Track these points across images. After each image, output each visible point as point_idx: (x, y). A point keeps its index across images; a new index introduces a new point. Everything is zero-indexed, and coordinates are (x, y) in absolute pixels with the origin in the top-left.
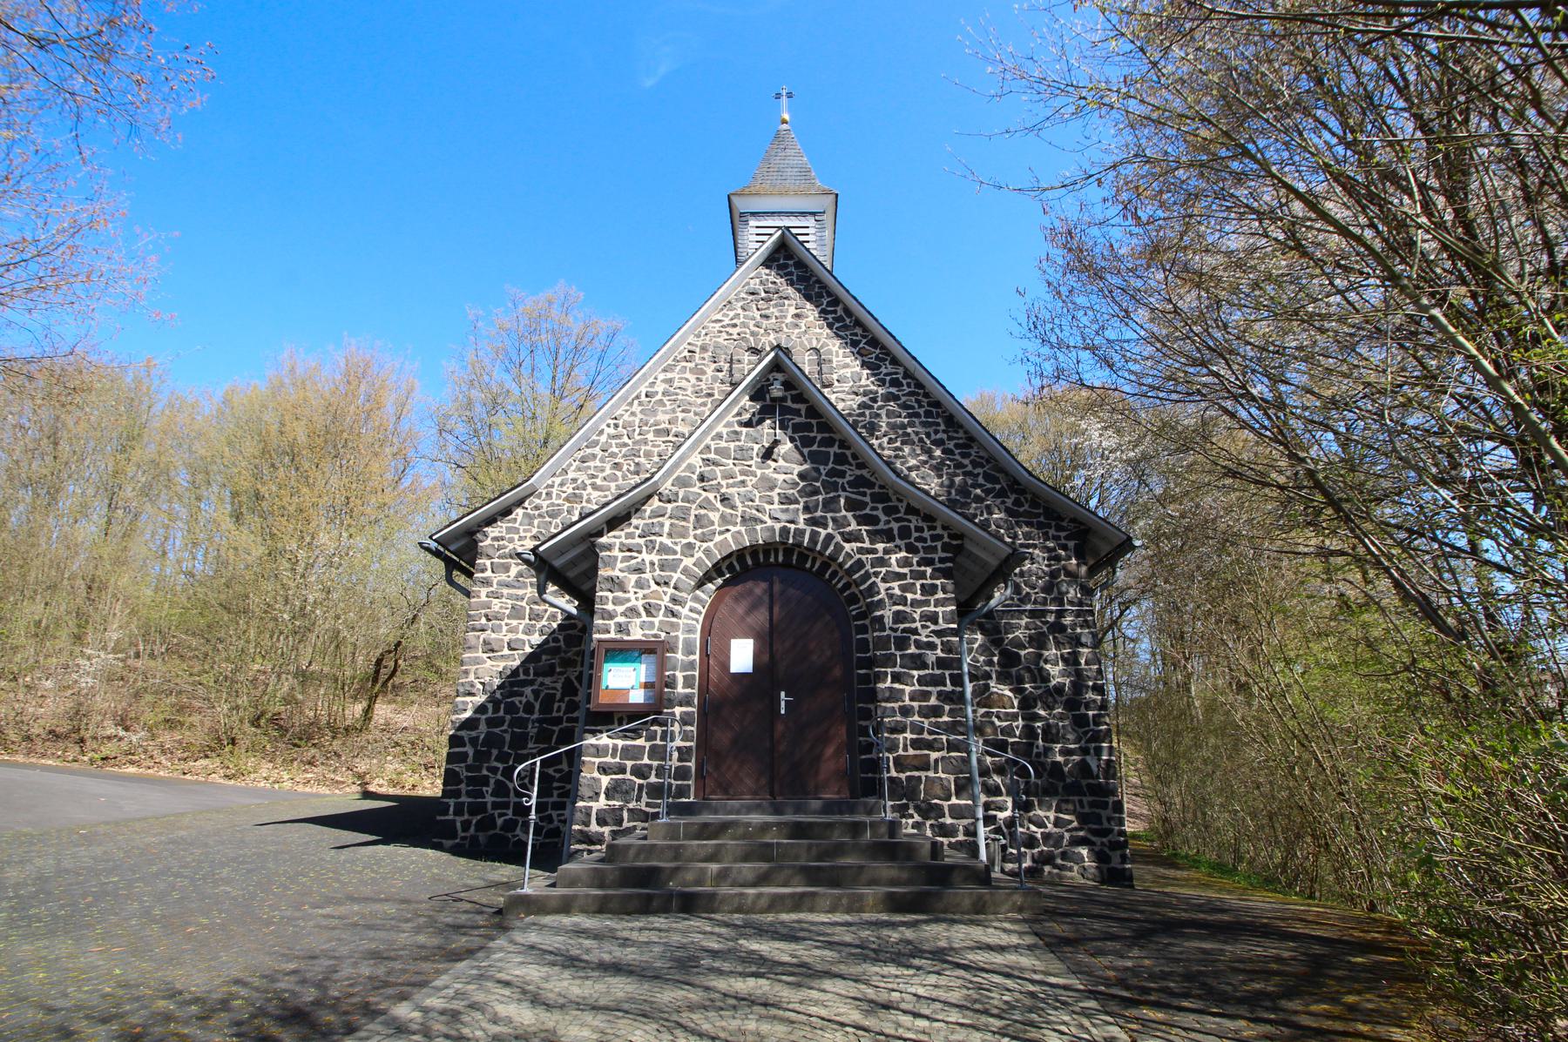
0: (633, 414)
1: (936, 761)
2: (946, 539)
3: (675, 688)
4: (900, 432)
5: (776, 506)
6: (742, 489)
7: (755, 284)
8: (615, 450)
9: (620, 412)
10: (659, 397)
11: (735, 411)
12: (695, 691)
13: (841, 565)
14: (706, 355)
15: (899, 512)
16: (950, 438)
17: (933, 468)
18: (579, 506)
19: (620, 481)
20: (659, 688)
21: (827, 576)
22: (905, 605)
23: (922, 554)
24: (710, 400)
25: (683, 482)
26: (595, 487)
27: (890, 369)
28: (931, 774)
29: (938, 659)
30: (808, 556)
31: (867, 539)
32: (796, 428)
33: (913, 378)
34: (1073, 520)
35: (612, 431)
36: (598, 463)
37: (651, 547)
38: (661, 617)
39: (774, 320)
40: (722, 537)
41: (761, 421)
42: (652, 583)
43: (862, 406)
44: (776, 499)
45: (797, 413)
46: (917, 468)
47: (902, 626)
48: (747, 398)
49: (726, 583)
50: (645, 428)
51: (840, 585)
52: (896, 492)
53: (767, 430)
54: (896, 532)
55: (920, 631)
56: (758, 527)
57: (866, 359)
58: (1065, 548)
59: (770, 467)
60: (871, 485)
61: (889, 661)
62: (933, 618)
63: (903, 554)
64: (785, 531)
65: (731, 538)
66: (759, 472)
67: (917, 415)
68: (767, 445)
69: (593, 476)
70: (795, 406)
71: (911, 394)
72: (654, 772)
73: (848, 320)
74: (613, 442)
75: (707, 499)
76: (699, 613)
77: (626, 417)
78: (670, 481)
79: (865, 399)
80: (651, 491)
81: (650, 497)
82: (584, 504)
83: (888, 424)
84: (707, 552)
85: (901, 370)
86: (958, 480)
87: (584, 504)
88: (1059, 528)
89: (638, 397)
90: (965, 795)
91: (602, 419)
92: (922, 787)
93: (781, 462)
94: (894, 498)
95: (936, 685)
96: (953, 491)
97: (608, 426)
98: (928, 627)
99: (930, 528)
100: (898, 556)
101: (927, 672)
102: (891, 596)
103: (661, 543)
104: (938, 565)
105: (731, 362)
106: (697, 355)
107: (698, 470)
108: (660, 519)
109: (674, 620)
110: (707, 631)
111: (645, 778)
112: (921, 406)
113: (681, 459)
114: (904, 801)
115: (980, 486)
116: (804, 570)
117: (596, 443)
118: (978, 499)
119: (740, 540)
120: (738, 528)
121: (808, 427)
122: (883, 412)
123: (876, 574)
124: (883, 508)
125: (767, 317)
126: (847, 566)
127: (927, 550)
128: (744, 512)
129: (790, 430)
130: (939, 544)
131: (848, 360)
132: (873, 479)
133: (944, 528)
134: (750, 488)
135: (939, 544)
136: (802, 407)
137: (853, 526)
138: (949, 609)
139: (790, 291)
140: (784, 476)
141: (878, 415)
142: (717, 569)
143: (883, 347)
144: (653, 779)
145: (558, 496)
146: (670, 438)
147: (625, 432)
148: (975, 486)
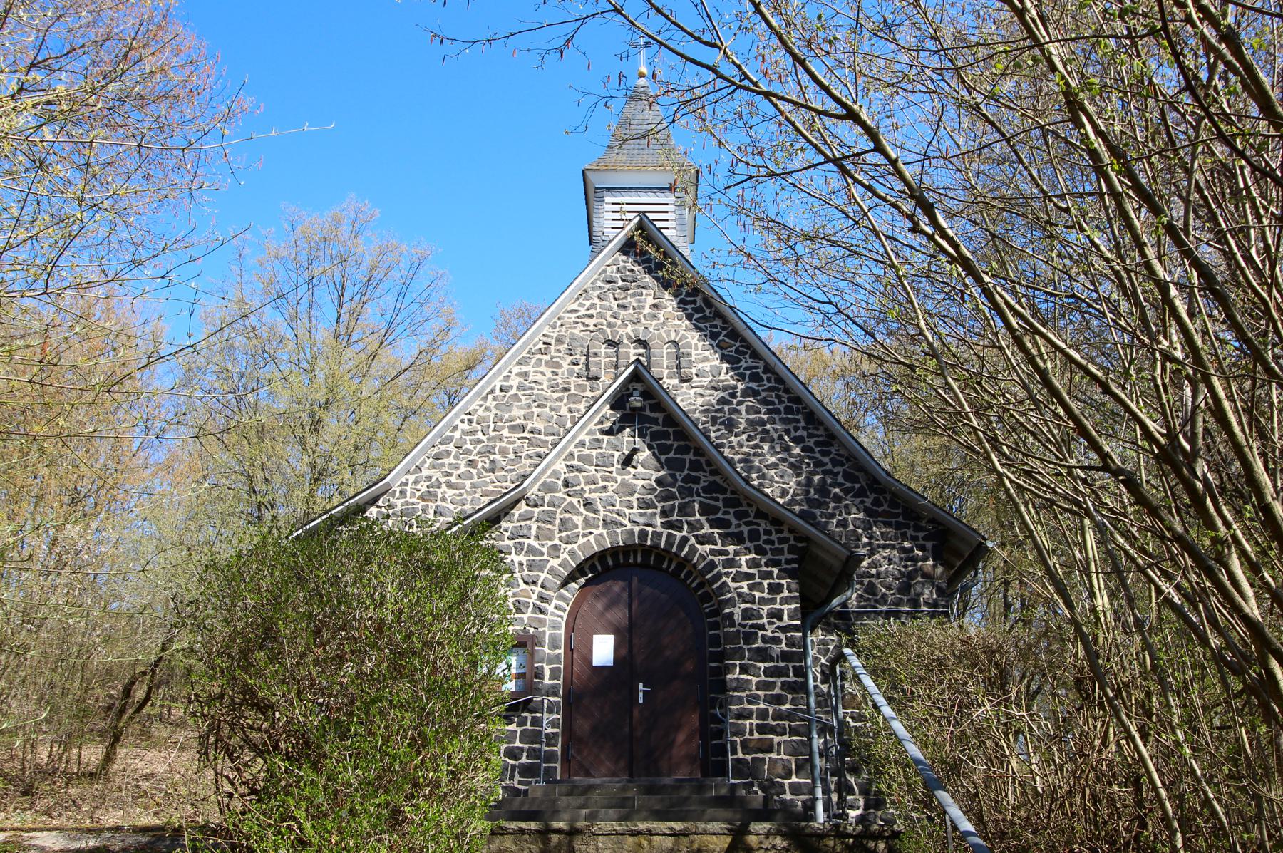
0: (487, 409)
1: (779, 744)
2: (792, 542)
3: (543, 679)
4: (760, 429)
5: (635, 510)
6: (604, 494)
7: (611, 272)
8: (470, 447)
9: (473, 407)
10: (514, 391)
11: (597, 419)
12: (561, 682)
13: (695, 566)
14: (561, 348)
15: (749, 516)
16: (810, 436)
17: (792, 466)
18: (433, 505)
19: (475, 480)
20: (530, 679)
21: (682, 576)
22: (753, 603)
23: (769, 556)
24: (566, 394)
25: (548, 488)
26: (450, 485)
27: (750, 363)
28: (774, 756)
29: (783, 652)
30: (665, 558)
31: (719, 542)
32: (655, 436)
33: (774, 373)
34: (932, 521)
35: (465, 426)
36: (452, 460)
38: (529, 614)
39: (631, 311)
40: (586, 539)
41: (621, 430)
42: (521, 582)
43: (722, 401)
44: (635, 504)
45: (655, 421)
46: (775, 466)
47: (751, 622)
48: (608, 407)
49: (588, 582)
50: (499, 424)
51: (694, 585)
52: (746, 498)
53: (627, 438)
54: (746, 535)
55: (767, 627)
56: (619, 530)
57: (726, 352)
58: (922, 548)
59: (629, 473)
60: (724, 491)
61: (739, 654)
62: (778, 615)
63: (753, 555)
64: (643, 534)
66: (619, 478)
67: (777, 411)
68: (627, 452)
69: (448, 474)
70: (653, 415)
72: (525, 754)
73: (707, 311)
74: (468, 438)
75: (571, 503)
76: (564, 610)
77: (480, 412)
78: (536, 487)
79: (723, 394)
80: (519, 496)
81: (518, 501)
82: (439, 502)
85: (761, 364)
86: (816, 478)
87: (439, 502)
89: (492, 391)
90: (803, 773)
91: (456, 416)
92: (766, 767)
93: (640, 469)
94: (744, 503)
95: (779, 676)
96: (812, 491)
97: (462, 421)
98: (773, 623)
99: (778, 532)
100: (748, 557)
101: (772, 664)
102: (740, 595)
103: (529, 545)
104: (785, 566)
105: (588, 355)
106: (552, 348)
107: (563, 477)
108: (528, 522)
109: (542, 616)
110: (571, 628)
111: (517, 759)
112: (781, 402)
113: (548, 466)
114: (750, 780)
115: (839, 485)
116: (661, 570)
117: (450, 439)
118: (837, 499)
119: (603, 543)
120: (600, 531)
121: (665, 435)
122: (743, 408)
123: (727, 574)
124: (734, 513)
125: (624, 307)
126: (700, 567)
127: (775, 552)
128: (606, 516)
129: (648, 438)
130: (785, 547)
131: (707, 353)
132: (725, 485)
133: (791, 531)
134: (611, 493)
135: (785, 547)
136: (660, 416)
137: (707, 530)
138: (793, 606)
139: (648, 279)
140: (643, 482)
141: (738, 412)
143: (743, 340)
144: (524, 760)
145: (413, 494)
146: (526, 434)
147: (479, 428)
148: (834, 485)
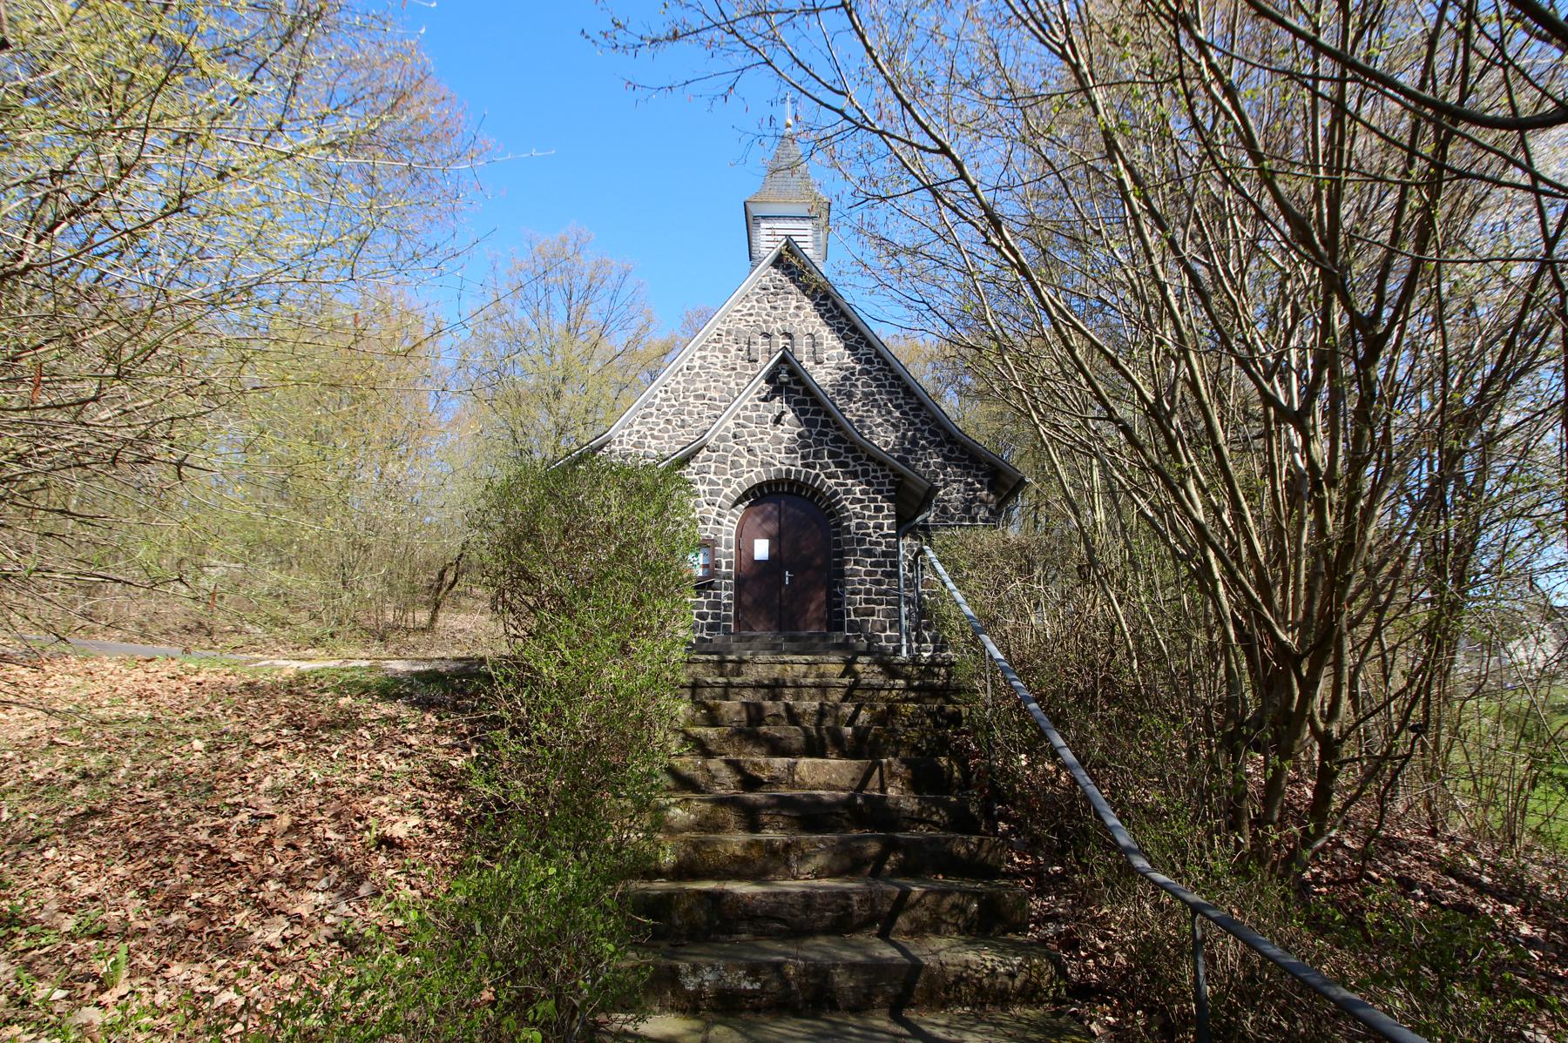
0: (678, 383)
5: (783, 455)
7: (766, 281)
8: (666, 409)
10: (696, 370)
16: (906, 403)
20: (712, 568)
25: (722, 439)
26: (653, 437)
27: (866, 350)
32: (797, 403)
33: (882, 357)
34: (989, 463)
35: (663, 395)
36: (654, 419)
37: (703, 481)
41: (773, 398)
43: (845, 378)
45: (797, 392)
49: (751, 504)
53: (777, 404)
64: (788, 472)
65: (756, 475)
67: (884, 386)
69: (652, 429)
71: (879, 370)
77: (673, 385)
81: (701, 448)
83: (863, 392)
84: (739, 484)
85: (873, 351)
88: (978, 469)
91: (656, 387)
93: (786, 426)
105: (749, 344)
110: (739, 534)
113: (722, 424)
115: (926, 439)
118: (924, 448)
121: (804, 402)
125: (775, 308)
131: (835, 343)
133: (891, 470)
136: (800, 388)
137: (833, 469)
139: (793, 287)
142: (745, 496)
144: (709, 620)
145: (628, 443)
